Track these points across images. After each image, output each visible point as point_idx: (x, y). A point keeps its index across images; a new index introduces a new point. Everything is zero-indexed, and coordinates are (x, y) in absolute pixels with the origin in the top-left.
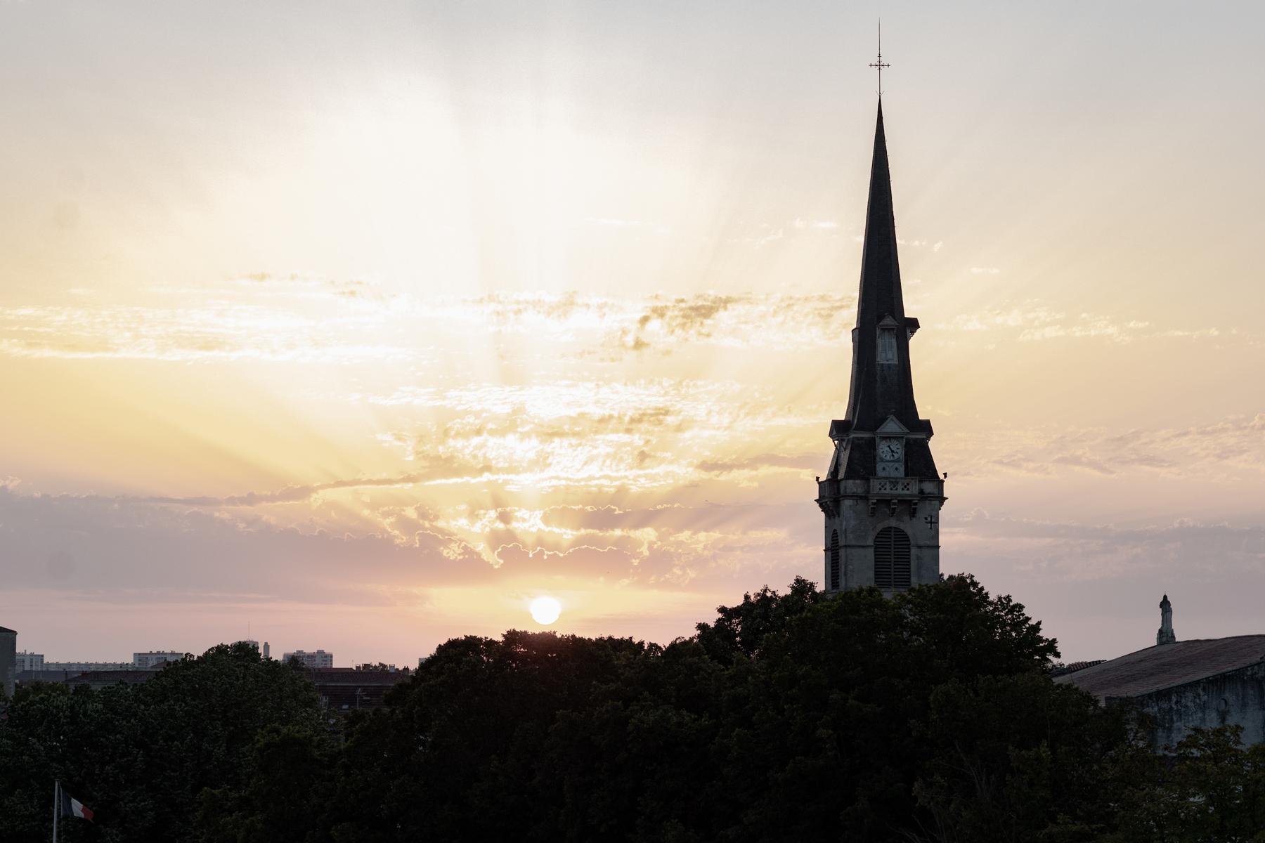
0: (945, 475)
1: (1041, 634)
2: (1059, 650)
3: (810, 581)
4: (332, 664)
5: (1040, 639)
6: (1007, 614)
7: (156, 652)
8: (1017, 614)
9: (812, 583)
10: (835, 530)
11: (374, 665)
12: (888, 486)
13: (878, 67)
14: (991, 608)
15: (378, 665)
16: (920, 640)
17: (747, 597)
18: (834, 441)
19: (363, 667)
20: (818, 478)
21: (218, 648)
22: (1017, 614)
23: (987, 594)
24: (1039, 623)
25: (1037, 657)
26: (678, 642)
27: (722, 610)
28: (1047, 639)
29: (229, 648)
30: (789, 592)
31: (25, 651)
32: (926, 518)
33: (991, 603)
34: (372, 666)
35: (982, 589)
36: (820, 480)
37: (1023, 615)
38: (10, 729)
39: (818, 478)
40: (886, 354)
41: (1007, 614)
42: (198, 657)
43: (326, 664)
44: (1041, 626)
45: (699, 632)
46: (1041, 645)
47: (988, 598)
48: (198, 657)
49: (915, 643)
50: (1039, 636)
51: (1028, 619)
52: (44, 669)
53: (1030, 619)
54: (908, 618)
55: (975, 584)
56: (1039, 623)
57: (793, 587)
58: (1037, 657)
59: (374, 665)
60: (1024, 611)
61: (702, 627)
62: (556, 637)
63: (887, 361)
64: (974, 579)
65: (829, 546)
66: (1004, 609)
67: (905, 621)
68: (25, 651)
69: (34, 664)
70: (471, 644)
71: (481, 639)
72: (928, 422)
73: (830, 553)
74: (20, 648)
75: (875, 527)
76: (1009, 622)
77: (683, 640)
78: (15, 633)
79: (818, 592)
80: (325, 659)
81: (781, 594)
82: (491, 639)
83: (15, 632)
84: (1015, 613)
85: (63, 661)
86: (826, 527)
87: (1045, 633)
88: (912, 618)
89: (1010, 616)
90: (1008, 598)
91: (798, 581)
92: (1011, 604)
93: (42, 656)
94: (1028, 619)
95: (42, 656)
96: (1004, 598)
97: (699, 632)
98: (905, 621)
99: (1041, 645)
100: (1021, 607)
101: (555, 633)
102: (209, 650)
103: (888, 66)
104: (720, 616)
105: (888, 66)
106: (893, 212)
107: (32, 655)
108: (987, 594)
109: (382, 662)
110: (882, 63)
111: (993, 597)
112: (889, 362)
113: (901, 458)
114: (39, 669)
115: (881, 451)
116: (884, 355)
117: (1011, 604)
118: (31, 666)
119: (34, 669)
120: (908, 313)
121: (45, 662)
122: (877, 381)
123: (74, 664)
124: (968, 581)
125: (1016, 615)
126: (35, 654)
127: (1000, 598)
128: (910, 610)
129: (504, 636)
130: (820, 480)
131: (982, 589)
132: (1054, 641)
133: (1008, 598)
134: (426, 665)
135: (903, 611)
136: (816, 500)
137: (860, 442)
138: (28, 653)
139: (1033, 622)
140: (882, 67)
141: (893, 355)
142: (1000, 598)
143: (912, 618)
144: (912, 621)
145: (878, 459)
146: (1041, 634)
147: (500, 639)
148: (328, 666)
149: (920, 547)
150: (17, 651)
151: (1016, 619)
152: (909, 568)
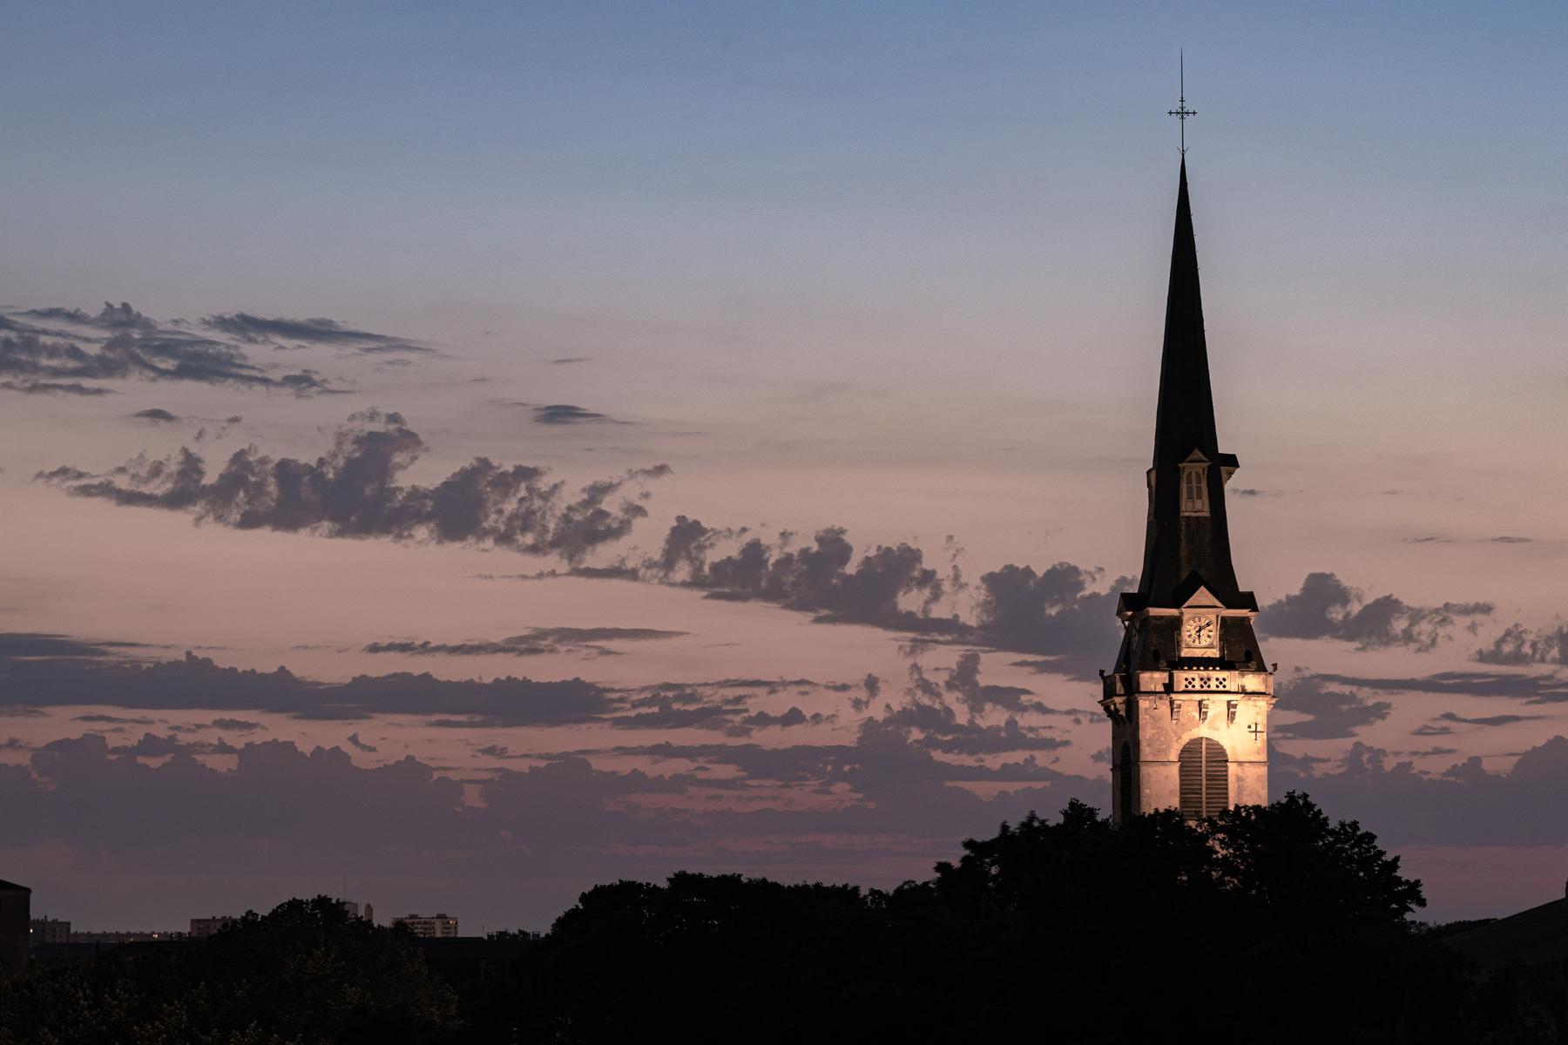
0: (1275, 666)
1: (1399, 873)
2: (1424, 895)
3: (1090, 806)
4: (456, 933)
5: (1399, 881)
6: (1352, 847)
7: (220, 918)
8: (1366, 846)
9: (1093, 809)
10: (1126, 742)
11: (511, 933)
12: (1197, 684)
13: (1179, 116)
14: (1331, 839)
15: (517, 932)
16: (1233, 882)
17: (1005, 828)
18: (1123, 622)
19: (498, 936)
20: (1102, 672)
21: (289, 903)
22: (1366, 846)
23: (1326, 819)
24: (1397, 859)
25: (1394, 906)
26: (906, 887)
27: (969, 844)
28: (1408, 881)
29: (304, 903)
30: (1061, 820)
31: (46, 917)
32: (1249, 727)
33: (1332, 832)
34: (509, 935)
35: (1320, 812)
36: (1105, 674)
37: (1375, 847)
38: (13, 1015)
39: (1102, 672)
40: (1194, 506)
41: (1352, 847)
42: (263, 917)
43: (449, 933)
44: (1399, 864)
45: (938, 875)
46: (1400, 888)
47: (1328, 825)
48: (263, 917)
49: (1228, 887)
50: (1397, 876)
51: (1382, 853)
52: (71, 941)
53: (1385, 853)
54: (1218, 852)
55: (1309, 806)
56: (1397, 859)
57: (1065, 814)
58: (1394, 906)
59: (511, 933)
60: (1376, 843)
61: (942, 867)
62: (741, 882)
63: (1196, 512)
64: (1309, 799)
65: (1118, 763)
66: (1349, 840)
67: (1215, 856)
68: (46, 917)
69: (57, 934)
70: (628, 890)
71: (641, 885)
72: (1425, 900)
73: (1118, 774)
74: (35, 913)
75: (1180, 738)
76: (1356, 857)
77: (913, 885)
78: (28, 891)
79: (1099, 820)
80: (447, 926)
81: (1051, 823)
82: (655, 885)
83: (29, 889)
84: (1364, 845)
85: (97, 930)
86: (1113, 738)
87: (1404, 873)
88: (1225, 852)
89: (1356, 850)
90: (1355, 825)
91: (1074, 805)
92: (1359, 833)
93: (69, 924)
94: (1382, 853)
95: (69, 924)
96: (1349, 825)
97: (938, 875)
98: (1215, 856)
99: (1400, 888)
100: (1370, 837)
101: (739, 876)
102: (278, 908)
103: (1194, 113)
104: (967, 852)
105: (1194, 113)
106: (1201, 311)
107: (55, 921)
108: (1326, 819)
109: (522, 929)
110: (1185, 110)
111: (1333, 824)
112: (1198, 514)
113: (1215, 644)
114: (65, 941)
115: (1188, 633)
116: (1190, 505)
117: (1359, 833)
118: (54, 936)
119: (58, 940)
120: (1223, 448)
121: (72, 932)
122: (1181, 539)
123: (111, 934)
124: (1301, 802)
125: (1365, 848)
126: (59, 920)
127: (1343, 825)
128: (1222, 841)
129: (669, 880)
130: (1105, 674)
131: (1320, 812)
132: (1417, 883)
133: (1355, 825)
134: (565, 924)
135: (1211, 843)
136: (1099, 702)
137: (1159, 622)
138: (49, 920)
139: (1388, 857)
140: (1185, 116)
141: (1203, 505)
142: (1343, 825)
143: (1225, 852)
144: (1224, 857)
145: (1183, 646)
146: (1399, 873)
147: (664, 884)
148: (453, 935)
149: (1240, 763)
150: (32, 918)
151: (1365, 853)
152: (1227, 794)
